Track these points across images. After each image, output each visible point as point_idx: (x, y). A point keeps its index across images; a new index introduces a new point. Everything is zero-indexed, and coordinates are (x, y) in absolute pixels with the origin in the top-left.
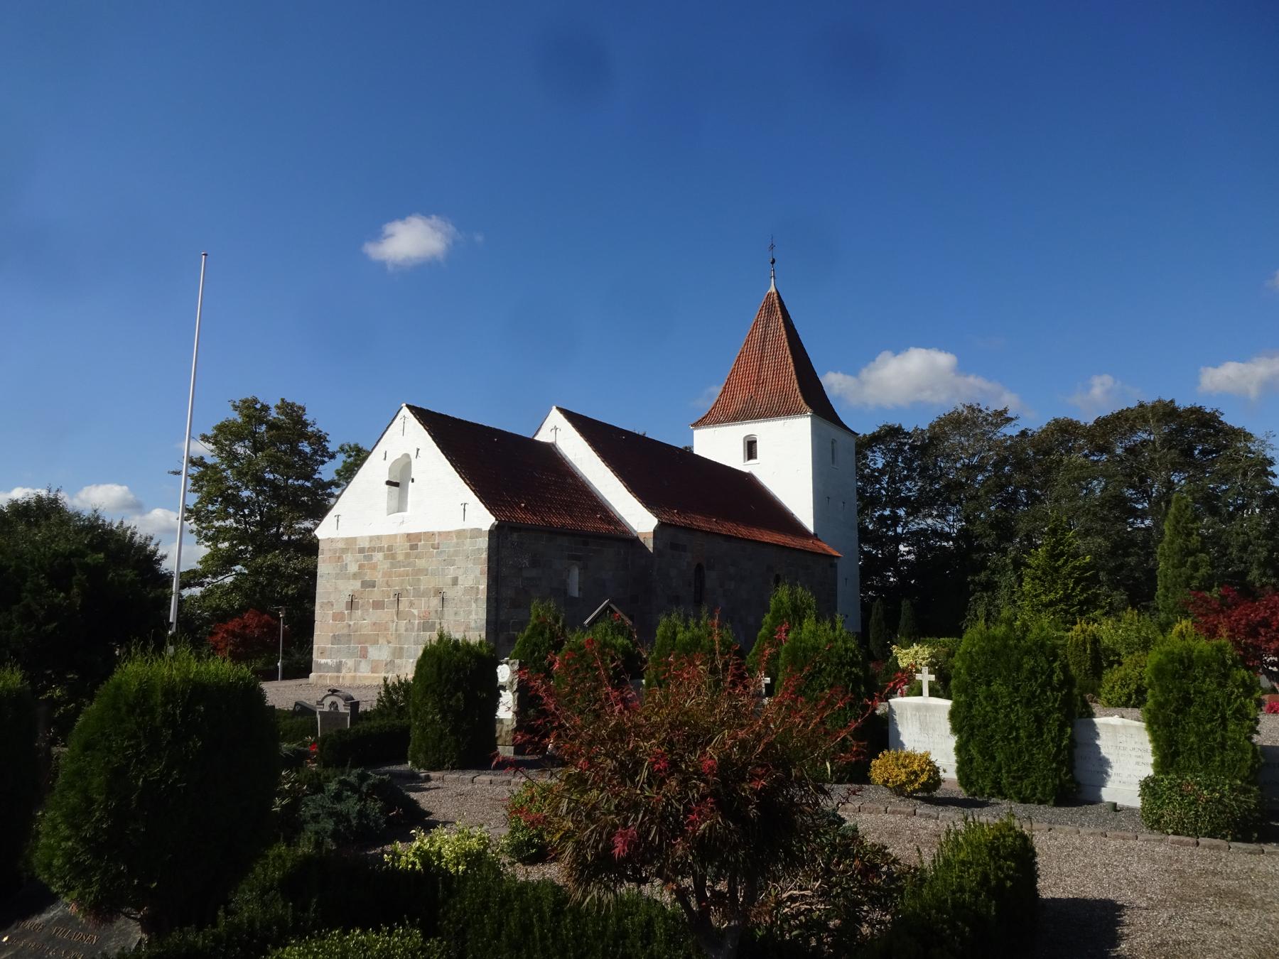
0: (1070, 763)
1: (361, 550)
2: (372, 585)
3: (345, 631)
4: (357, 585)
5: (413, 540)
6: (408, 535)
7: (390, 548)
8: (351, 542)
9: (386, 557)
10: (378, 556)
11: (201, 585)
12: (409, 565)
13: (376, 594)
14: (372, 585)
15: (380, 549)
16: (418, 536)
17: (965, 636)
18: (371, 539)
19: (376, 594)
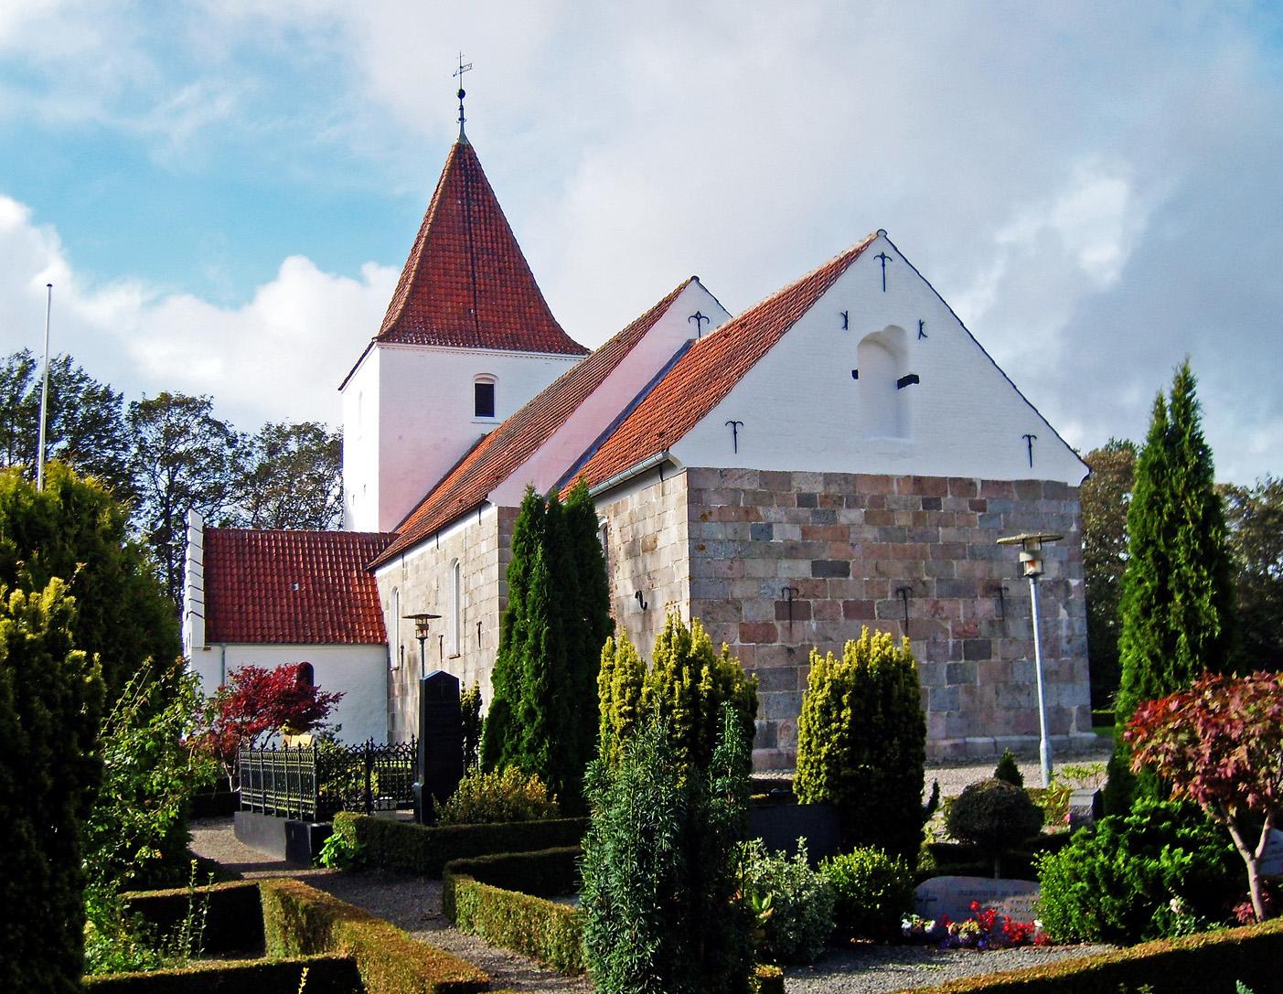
0: (540, 302)
1: (806, 500)
2: (842, 569)
3: (780, 662)
4: (803, 568)
5: (928, 491)
6: (918, 481)
7: (878, 502)
8: (775, 483)
9: (869, 518)
10: (848, 516)
11: (1177, 634)
12: (923, 537)
13: (853, 588)
14: (842, 569)
15: (853, 503)
16: (940, 484)
17: (617, 630)
18: (829, 478)
19: (853, 588)
